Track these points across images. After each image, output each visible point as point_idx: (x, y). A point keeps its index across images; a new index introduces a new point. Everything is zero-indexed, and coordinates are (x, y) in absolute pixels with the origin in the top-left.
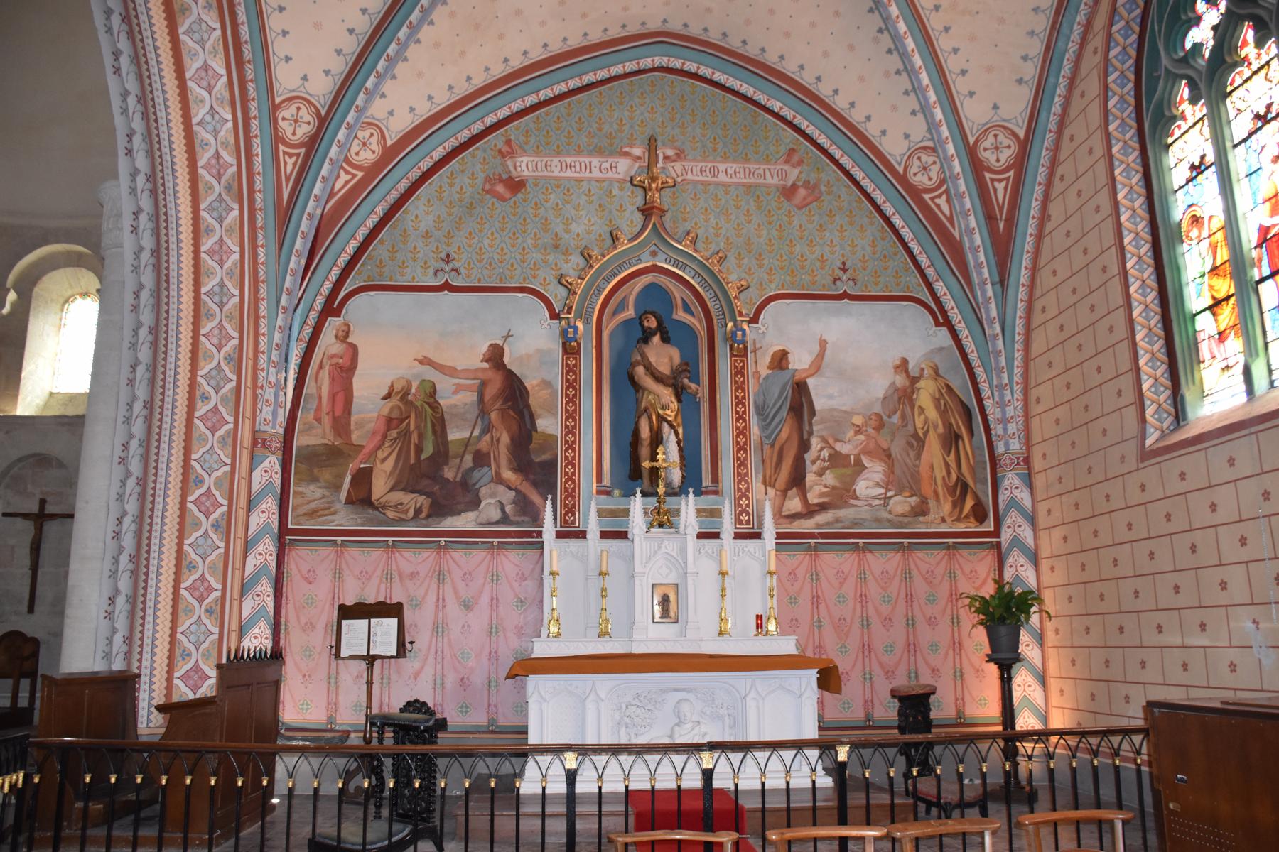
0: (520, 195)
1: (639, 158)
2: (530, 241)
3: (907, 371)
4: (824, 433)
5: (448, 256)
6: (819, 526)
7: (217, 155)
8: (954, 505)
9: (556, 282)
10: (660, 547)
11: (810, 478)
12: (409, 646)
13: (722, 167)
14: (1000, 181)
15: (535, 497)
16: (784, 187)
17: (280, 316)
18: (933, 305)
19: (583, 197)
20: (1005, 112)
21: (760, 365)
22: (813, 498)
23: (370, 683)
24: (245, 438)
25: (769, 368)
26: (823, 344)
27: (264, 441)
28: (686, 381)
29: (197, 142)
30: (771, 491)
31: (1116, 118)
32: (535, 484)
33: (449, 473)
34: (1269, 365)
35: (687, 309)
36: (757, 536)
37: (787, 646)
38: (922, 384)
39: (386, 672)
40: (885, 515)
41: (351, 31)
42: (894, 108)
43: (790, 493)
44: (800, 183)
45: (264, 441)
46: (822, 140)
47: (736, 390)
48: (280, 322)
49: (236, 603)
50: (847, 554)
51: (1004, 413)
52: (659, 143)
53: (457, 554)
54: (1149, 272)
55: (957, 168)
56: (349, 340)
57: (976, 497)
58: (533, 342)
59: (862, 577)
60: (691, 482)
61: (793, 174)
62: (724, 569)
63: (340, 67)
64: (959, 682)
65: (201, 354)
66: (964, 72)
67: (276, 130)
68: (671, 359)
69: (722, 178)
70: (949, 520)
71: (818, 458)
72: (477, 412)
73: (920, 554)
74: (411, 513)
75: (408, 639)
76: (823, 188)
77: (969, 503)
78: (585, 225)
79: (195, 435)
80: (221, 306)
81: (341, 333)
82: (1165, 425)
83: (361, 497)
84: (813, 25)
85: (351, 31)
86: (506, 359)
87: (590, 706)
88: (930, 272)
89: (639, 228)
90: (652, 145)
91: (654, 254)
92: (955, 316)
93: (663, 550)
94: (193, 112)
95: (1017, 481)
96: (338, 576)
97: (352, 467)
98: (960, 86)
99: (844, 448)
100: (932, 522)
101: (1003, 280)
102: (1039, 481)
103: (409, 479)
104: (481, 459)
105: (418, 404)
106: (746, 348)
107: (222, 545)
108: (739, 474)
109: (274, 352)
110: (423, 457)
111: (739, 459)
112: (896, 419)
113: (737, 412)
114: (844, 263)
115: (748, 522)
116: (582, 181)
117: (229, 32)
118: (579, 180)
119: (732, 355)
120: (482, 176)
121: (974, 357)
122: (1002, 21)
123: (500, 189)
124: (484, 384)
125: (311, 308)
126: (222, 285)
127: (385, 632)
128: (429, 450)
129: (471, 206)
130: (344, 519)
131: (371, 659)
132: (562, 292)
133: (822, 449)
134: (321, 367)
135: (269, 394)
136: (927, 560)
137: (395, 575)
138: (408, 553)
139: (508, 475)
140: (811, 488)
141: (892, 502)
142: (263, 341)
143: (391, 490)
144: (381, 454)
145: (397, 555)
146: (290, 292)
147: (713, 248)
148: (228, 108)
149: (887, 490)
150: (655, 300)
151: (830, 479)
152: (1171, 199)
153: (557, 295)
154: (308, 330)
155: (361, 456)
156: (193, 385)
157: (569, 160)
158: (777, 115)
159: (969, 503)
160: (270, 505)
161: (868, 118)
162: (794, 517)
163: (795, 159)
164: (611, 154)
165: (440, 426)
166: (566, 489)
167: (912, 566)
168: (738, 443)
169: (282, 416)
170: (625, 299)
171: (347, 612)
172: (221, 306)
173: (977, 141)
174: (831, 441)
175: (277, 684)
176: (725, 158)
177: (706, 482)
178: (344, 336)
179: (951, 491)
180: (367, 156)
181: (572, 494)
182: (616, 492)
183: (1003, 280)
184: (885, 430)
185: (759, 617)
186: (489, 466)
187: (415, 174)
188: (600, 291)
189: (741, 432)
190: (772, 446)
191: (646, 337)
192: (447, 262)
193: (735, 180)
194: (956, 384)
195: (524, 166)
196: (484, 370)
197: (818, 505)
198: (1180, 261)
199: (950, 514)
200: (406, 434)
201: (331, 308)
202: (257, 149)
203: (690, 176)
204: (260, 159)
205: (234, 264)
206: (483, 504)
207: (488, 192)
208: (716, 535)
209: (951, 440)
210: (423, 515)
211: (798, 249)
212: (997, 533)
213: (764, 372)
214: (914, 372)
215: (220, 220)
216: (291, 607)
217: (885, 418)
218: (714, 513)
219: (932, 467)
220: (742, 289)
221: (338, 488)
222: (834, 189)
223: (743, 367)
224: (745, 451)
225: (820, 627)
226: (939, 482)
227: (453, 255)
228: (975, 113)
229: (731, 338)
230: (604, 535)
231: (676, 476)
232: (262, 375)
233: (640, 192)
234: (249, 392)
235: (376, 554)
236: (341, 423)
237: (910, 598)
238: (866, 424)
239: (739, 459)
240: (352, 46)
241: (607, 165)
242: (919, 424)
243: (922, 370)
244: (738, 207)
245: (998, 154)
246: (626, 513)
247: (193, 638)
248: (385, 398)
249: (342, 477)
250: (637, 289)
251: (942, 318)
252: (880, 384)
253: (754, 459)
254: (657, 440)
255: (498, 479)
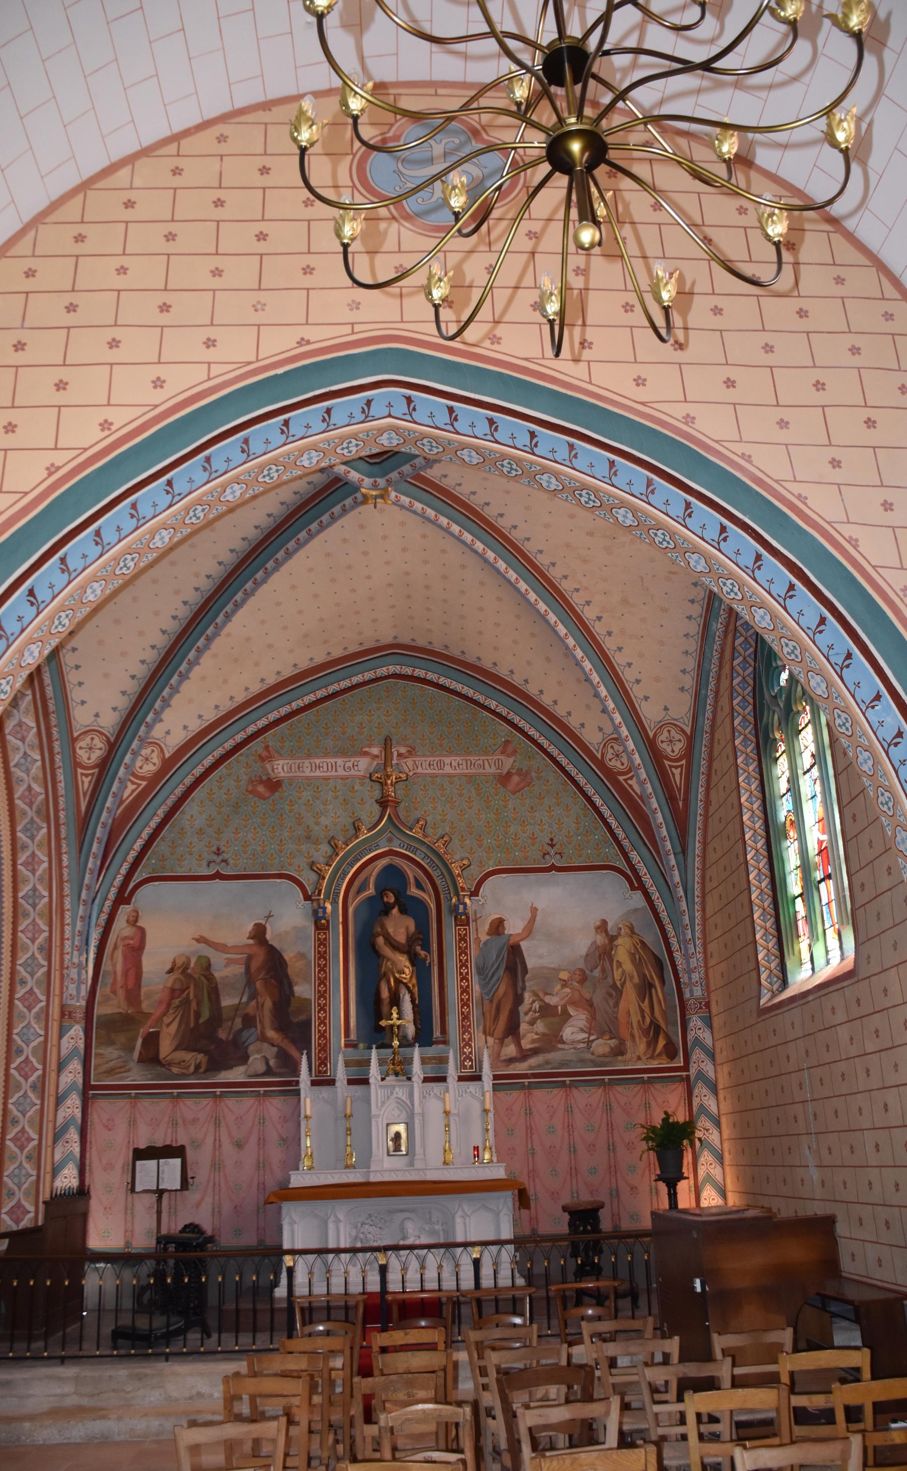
0: (277, 794)
1: (377, 756)
2: (286, 834)
3: (606, 931)
4: (535, 988)
5: (218, 849)
6: (531, 1068)
7: (29, 788)
8: (649, 1044)
9: (308, 868)
10: (392, 1093)
11: (524, 1027)
12: (190, 1181)
13: (447, 760)
14: (676, 767)
15: (293, 1052)
16: (500, 776)
17: (81, 907)
18: (629, 872)
19: (331, 793)
20: (674, 713)
21: (481, 932)
22: (526, 1044)
23: (159, 1213)
24: (55, 1012)
25: (488, 934)
26: (534, 911)
27: (70, 1013)
28: (418, 948)
29: (14, 780)
30: (490, 1040)
31: (741, 734)
32: (293, 1041)
33: (222, 1034)
34: (826, 947)
35: (419, 886)
36: (478, 1078)
37: (499, 1172)
38: (619, 941)
39: (173, 1203)
40: (589, 1056)
41: (133, 677)
42: (588, 707)
43: (506, 1040)
44: (514, 771)
45: (70, 1013)
46: (532, 732)
47: (460, 955)
48: (81, 913)
49: (49, 1149)
50: (555, 1091)
51: (688, 963)
52: (394, 742)
53: (230, 1102)
54: (763, 862)
55: (637, 759)
56: (139, 924)
57: (667, 1037)
58: (289, 920)
59: (569, 1110)
60: (424, 1037)
61: (508, 763)
62: (448, 1108)
63: (124, 703)
64: (654, 1198)
65: (19, 946)
66: (638, 681)
67: (75, 757)
68: (407, 928)
69: (448, 770)
70: (644, 1058)
71: (530, 1010)
72: (245, 982)
73: (619, 1088)
74: (192, 1069)
75: (190, 1174)
76: (534, 774)
77: (661, 1043)
78: (332, 818)
79: (16, 1013)
80: (34, 906)
81: (131, 919)
82: (775, 987)
83: (151, 1056)
84: (515, 642)
85: (133, 677)
86: (268, 936)
87: (331, 1226)
88: (626, 843)
89: (377, 818)
90: (387, 744)
91: (390, 840)
92: (647, 880)
93: (395, 1095)
94: (11, 758)
95: (699, 1023)
96: (132, 1123)
97: (142, 1031)
98: (636, 692)
99: (552, 1000)
100: (630, 1060)
101: (683, 851)
102: (716, 1022)
103: (191, 1039)
104: (249, 1021)
105: (196, 976)
106: (468, 918)
107: (38, 1102)
108: (463, 1026)
109: (77, 938)
110: (201, 1021)
111: (463, 1013)
112: (597, 973)
113: (461, 974)
114: (552, 840)
115: (471, 1067)
116: (329, 775)
117: (38, 696)
118: (326, 779)
119: (456, 925)
120: (245, 778)
121: (664, 915)
122: (662, 643)
123: (261, 789)
124: (250, 958)
125: (106, 899)
126: (34, 889)
127: (171, 1171)
128: (206, 1015)
129: (236, 806)
130: (136, 1075)
131: (160, 1192)
132: (313, 877)
133: (534, 1002)
134: (115, 947)
135: (74, 973)
136: (626, 1094)
137: (180, 1121)
138: (189, 1102)
139: (271, 1034)
140: (524, 1035)
141: (594, 1045)
142: (68, 929)
143: (174, 1050)
144: (167, 1020)
145: (181, 1104)
146: (89, 888)
147: (440, 832)
148: (38, 752)
149: (590, 1034)
150: (392, 878)
151: (540, 1027)
152: (779, 803)
153: (307, 879)
154: (104, 917)
155: (149, 1023)
156: (13, 972)
157: (317, 761)
158: (493, 712)
159: (661, 1043)
160: (76, 1065)
161: (569, 713)
162: (511, 1061)
163: (510, 749)
164: (352, 756)
165: (214, 994)
166: (319, 1045)
167: (612, 1099)
168: (462, 1000)
169: (84, 991)
170: (367, 880)
171: (140, 1154)
172: (34, 906)
173: (655, 735)
174: (541, 995)
175: (85, 1216)
176: (450, 753)
177: (437, 1033)
178: (133, 921)
179: (646, 1032)
180: (149, 769)
181: (324, 1047)
182: (361, 1046)
183: (683, 851)
184: (587, 983)
185: (476, 1148)
186: (256, 1027)
187: (189, 780)
188: (345, 874)
189: (465, 990)
190: (491, 1001)
191: (386, 910)
192: (218, 855)
193: (458, 771)
194: (648, 940)
195: (281, 768)
196: (249, 946)
197: (531, 1050)
198: (785, 854)
199: (645, 1054)
200: (186, 1002)
201: (123, 898)
202: (60, 777)
203: (420, 770)
204: (62, 784)
205: (44, 871)
206: (251, 1059)
207: (250, 792)
208: (443, 1079)
209: (645, 989)
210: (202, 1070)
211: (512, 829)
212: (686, 1067)
213: (484, 938)
214: (612, 931)
215: (32, 838)
216: (94, 1149)
217: (587, 972)
218: (442, 1061)
219: (629, 1013)
220: (464, 868)
221: (132, 1049)
222: (543, 774)
223: (465, 935)
224: (468, 1007)
225: (533, 1154)
226: (635, 1026)
227: (223, 848)
228: (651, 713)
229: (454, 910)
230: (350, 1082)
231: (411, 1031)
232: (67, 957)
233: (377, 786)
234: (58, 973)
235: (164, 1103)
236: (133, 994)
237: (610, 1127)
238: (571, 978)
239: (463, 1013)
240: (133, 688)
241: (350, 764)
242: (617, 975)
243: (620, 929)
244: (461, 795)
245: (673, 747)
246: (368, 1062)
247: (16, 1180)
248: (169, 972)
249: (134, 1039)
250: (377, 871)
251: (636, 883)
252: (583, 944)
253: (475, 1013)
254: (395, 1001)
255: (263, 1038)
